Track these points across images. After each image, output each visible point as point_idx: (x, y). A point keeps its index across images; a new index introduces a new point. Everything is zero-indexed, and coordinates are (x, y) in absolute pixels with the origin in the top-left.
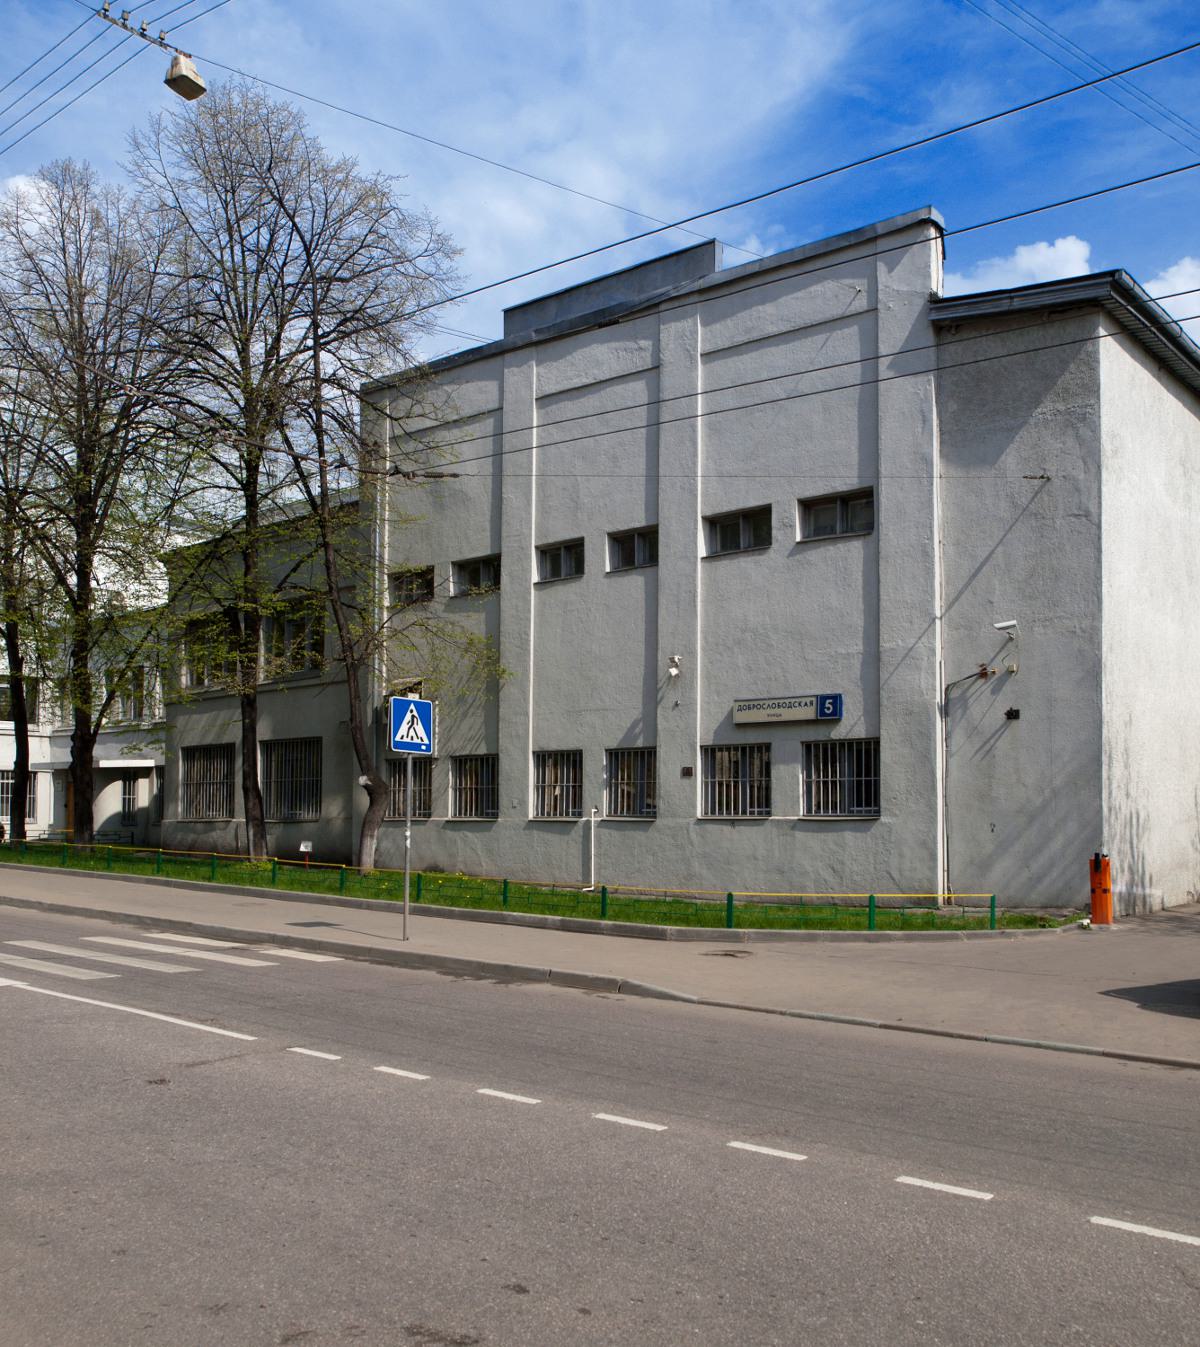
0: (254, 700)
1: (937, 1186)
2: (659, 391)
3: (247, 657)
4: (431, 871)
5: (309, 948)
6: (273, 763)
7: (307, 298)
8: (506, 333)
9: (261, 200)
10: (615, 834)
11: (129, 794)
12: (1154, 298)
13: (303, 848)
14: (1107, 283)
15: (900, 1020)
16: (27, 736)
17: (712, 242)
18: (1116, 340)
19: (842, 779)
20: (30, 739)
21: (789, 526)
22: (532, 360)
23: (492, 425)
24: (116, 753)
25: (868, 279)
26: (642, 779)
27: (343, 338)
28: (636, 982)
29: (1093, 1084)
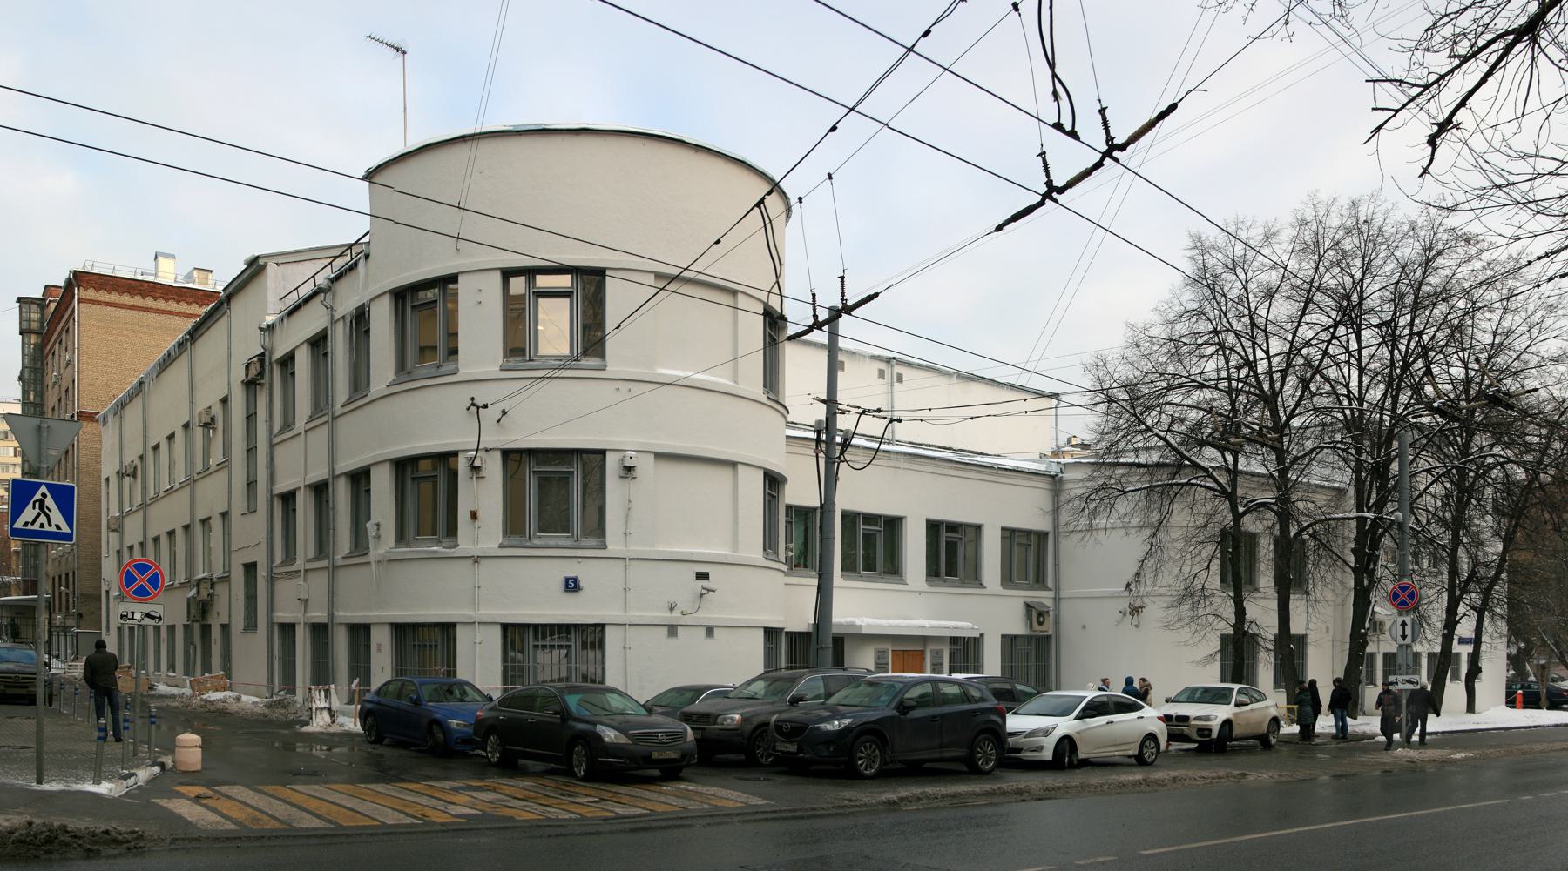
0: (369, 471)
1: (1346, 823)
2: (924, 627)
3: (44, 495)
4: (352, 682)
5: (419, 285)
6: (818, 553)
7: (1375, 596)
8: (1295, 636)
9: (1491, 450)
10: (53, 702)
11: (795, 663)
12: (200, 486)
13: (1292, 646)
14: (1236, 740)
15: (474, 516)
16: (606, 275)
17: (210, 518)
18: (784, 398)
19: (513, 673)
20: (834, 590)
21: (1043, 597)
22: (517, 762)
23: (955, 692)
24: (21, 593)
25: (1314, 732)
26: (419, 666)
27: (1461, 360)
28: (1096, 718)
29: (1333, 468)
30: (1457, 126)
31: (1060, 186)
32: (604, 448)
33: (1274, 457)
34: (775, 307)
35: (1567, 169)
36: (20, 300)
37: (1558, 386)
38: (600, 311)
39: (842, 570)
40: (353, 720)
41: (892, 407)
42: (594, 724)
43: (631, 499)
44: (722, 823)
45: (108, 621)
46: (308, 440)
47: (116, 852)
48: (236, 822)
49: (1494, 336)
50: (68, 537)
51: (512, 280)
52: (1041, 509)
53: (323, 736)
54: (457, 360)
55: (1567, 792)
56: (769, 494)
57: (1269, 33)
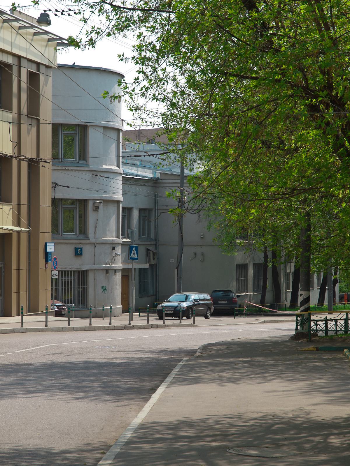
11: (81, 286)
20: (12, 52)
26: (79, 286)
30: (38, 4)
31: (39, 16)
32: (160, 321)
33: (171, 18)
34: (11, 23)
35: (125, 0)
36: (52, 183)
37: (225, 189)
38: (318, 311)
39: (140, 269)
40: (59, 51)
41: (153, 295)
42: (317, 349)
43: (161, 136)
44: (40, 396)
45: (281, 321)
46: (96, 250)
47: (36, 452)
48: (23, 110)
49: (163, 94)
50: (137, 259)
51: (333, 322)
52: (119, 60)
53: (68, 365)
54: (143, 407)
55: (349, 422)
56: (29, 87)
57: (95, 173)
